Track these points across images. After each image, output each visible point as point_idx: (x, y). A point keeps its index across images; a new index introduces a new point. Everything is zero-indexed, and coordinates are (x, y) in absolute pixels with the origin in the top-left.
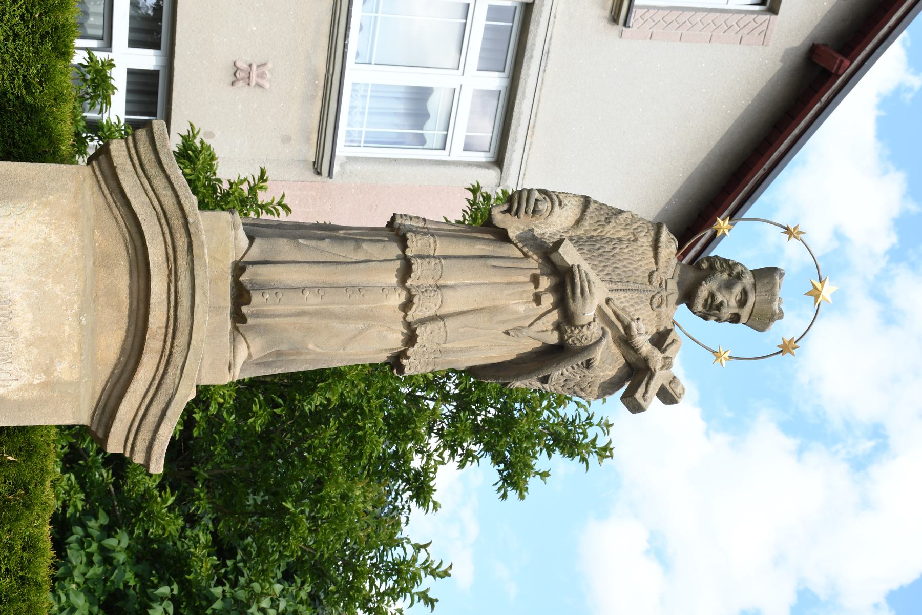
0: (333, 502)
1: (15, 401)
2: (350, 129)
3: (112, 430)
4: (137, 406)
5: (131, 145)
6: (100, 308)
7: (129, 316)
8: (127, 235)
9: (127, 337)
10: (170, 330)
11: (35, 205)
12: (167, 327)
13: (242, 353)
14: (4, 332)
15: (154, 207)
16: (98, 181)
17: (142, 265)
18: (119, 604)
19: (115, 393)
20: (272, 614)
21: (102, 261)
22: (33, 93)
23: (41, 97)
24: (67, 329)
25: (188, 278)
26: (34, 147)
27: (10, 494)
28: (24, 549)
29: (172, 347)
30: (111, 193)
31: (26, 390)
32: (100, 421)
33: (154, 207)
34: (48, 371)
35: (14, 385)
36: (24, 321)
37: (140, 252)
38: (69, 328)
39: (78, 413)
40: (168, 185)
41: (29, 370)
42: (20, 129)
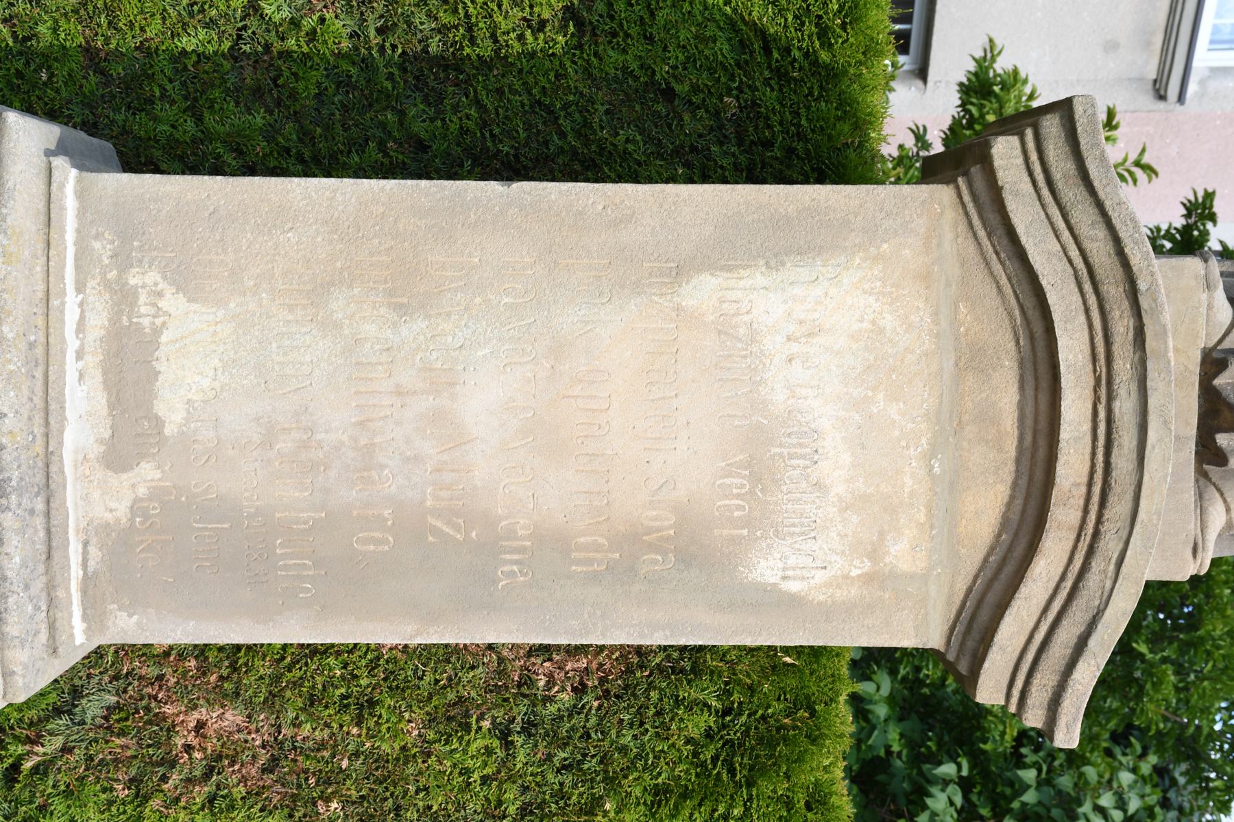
0: (1219, 648)
1: (820, 603)
2: (1218, 21)
3: (986, 665)
4: (1031, 625)
5: (1031, 145)
6: (965, 444)
7: (1018, 461)
8: (1017, 312)
9: (1012, 497)
10: (1097, 489)
11: (858, 261)
12: (1090, 484)
13: (1217, 518)
14: (804, 485)
15: (1070, 261)
16: (967, 214)
17: (1043, 368)
18: (881, 778)
19: (992, 598)
20: (1117, 815)
21: (971, 360)
22: (831, 45)
23: (842, 53)
24: (908, 481)
25: (1135, 394)
26: (830, 137)
27: (787, 716)
28: (808, 807)
29: (1099, 521)
30: (989, 235)
31: (839, 586)
32: (962, 644)
33: (1070, 261)
34: (875, 554)
35: (820, 577)
36: (837, 467)
37: (1041, 344)
38: (911, 480)
39: (919, 626)
40: (1099, 219)
41: (843, 552)
42: (808, 108)
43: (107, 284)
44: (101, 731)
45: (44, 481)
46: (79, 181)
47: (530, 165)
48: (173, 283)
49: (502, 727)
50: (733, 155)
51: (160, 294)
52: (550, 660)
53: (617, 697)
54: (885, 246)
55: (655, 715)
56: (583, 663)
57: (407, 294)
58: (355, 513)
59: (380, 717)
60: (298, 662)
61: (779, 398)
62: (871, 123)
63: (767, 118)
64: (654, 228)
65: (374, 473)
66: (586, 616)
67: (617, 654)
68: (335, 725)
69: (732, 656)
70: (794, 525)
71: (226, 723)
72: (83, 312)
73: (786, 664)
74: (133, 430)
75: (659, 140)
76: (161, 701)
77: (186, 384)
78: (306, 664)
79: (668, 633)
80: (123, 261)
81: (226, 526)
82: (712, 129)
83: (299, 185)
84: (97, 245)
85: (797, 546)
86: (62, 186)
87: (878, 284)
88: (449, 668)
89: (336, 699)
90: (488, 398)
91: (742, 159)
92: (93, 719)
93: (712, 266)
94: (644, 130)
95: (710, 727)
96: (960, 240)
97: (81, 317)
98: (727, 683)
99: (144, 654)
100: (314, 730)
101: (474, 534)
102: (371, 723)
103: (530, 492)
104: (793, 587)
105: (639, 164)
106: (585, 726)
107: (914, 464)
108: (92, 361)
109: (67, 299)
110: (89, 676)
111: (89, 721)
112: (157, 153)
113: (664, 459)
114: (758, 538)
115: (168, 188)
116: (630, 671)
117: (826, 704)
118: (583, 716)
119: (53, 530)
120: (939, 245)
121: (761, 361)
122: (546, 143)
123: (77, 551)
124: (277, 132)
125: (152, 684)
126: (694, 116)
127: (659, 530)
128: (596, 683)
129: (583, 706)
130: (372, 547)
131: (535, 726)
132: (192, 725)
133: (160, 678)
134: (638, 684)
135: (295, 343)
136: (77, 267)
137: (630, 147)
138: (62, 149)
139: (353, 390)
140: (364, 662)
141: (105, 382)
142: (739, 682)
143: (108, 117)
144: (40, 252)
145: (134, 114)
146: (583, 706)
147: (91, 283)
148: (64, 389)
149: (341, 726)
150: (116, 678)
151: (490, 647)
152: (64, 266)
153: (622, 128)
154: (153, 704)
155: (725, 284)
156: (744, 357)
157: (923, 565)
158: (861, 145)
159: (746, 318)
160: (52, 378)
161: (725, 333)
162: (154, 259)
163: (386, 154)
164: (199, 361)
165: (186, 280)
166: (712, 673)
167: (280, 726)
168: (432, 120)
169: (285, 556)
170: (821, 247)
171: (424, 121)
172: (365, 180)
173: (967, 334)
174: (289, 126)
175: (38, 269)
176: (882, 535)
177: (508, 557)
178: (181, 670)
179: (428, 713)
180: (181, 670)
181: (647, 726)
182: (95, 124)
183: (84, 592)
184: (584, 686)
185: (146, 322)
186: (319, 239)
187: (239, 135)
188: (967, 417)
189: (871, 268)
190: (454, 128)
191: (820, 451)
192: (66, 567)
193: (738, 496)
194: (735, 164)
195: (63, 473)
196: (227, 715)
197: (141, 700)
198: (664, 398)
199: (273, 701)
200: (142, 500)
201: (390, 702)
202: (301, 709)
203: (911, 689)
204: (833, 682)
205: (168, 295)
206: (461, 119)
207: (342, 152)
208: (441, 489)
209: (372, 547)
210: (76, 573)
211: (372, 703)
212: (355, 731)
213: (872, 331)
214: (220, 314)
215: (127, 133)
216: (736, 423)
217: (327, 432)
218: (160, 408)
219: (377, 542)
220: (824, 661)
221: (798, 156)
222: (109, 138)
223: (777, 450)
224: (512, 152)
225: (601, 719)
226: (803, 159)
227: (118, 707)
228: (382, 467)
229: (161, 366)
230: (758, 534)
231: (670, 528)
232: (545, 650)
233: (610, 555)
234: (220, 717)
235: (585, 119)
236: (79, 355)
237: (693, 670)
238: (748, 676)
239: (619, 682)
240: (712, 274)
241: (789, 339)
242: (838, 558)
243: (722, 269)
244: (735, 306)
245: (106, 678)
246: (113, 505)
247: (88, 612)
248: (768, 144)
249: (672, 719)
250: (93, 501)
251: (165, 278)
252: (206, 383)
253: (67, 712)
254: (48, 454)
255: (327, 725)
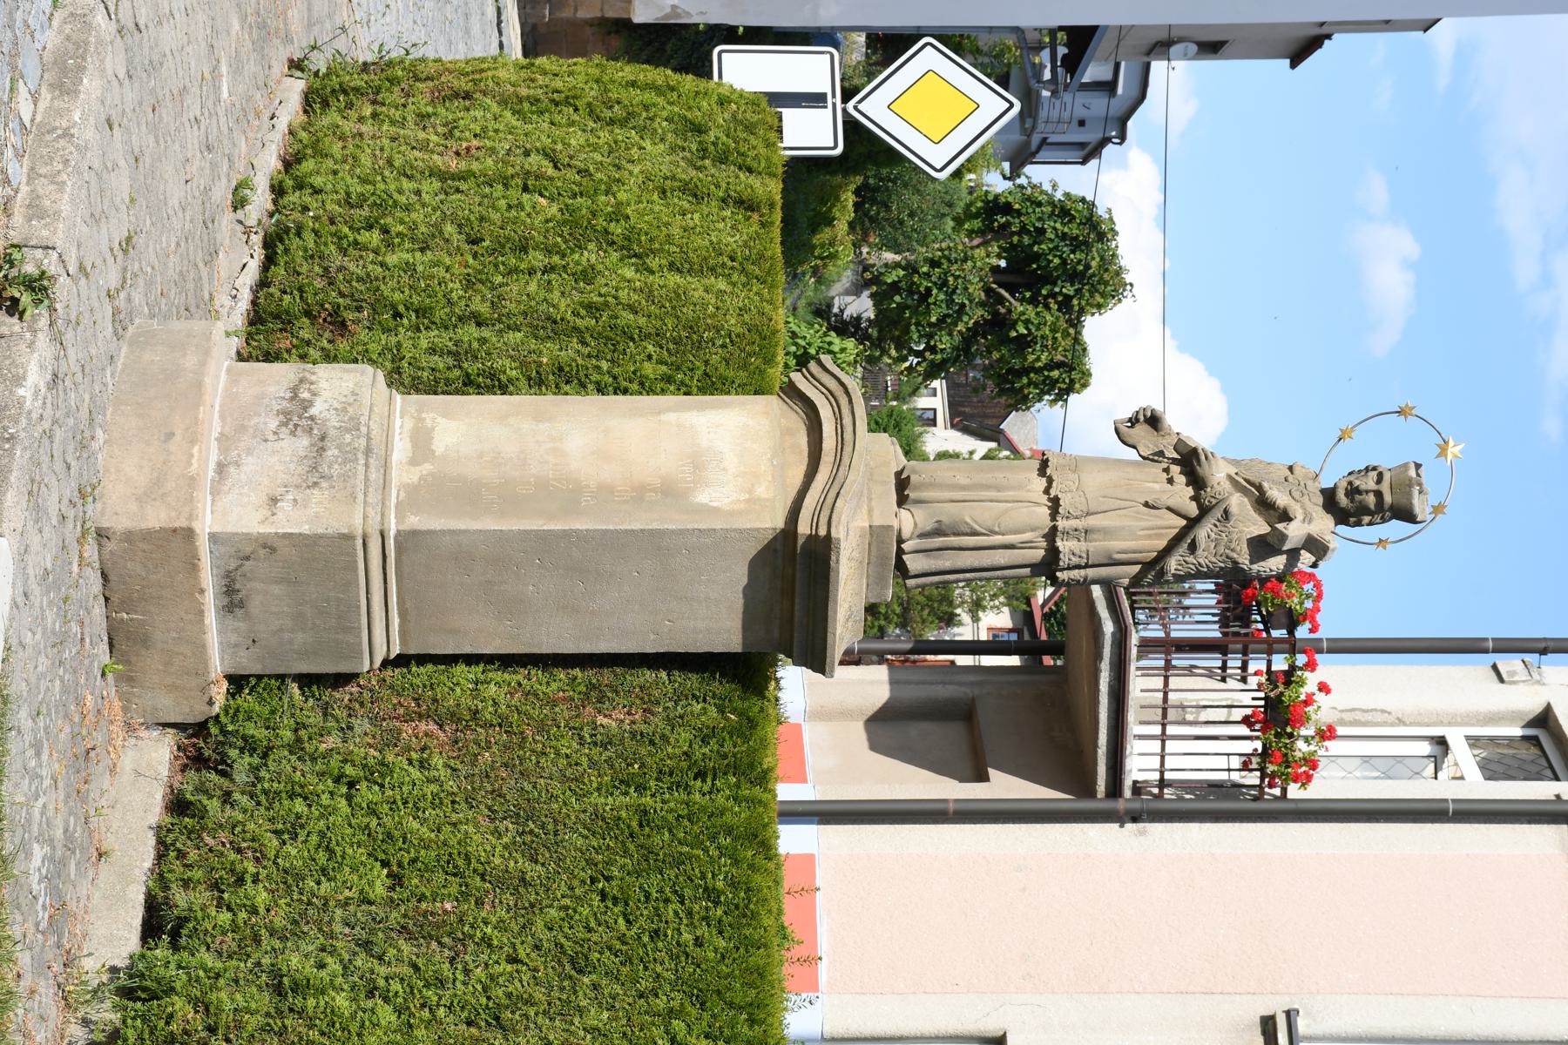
104: (715, 504)
210: (394, 500)
250: (402, 473)
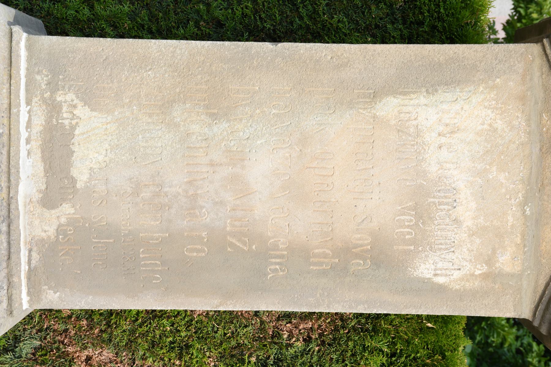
11: (481, 89)
14: (447, 220)
24: (510, 219)
26: (458, 19)
27: (429, 358)
31: (468, 280)
34: (490, 261)
35: (457, 275)
36: (467, 210)
38: (512, 218)
41: (471, 260)
43: (44, 100)
44: (31, 362)
45: (7, 214)
46: (28, 40)
47: (282, 35)
48: (82, 100)
49: (262, 362)
50: (400, 30)
51: (75, 107)
52: (290, 322)
53: (329, 345)
54: (498, 80)
55: (351, 356)
56: (310, 325)
57: (217, 107)
58: (186, 234)
59: (192, 354)
60: (145, 322)
61: (433, 169)
62: (482, 11)
63: (421, 8)
64: (360, 70)
65: (197, 211)
66: (318, 295)
67: (329, 320)
68: (166, 359)
69: (396, 322)
70: (441, 244)
71: (104, 357)
72: (30, 116)
73: (428, 328)
74: (58, 185)
75: (357, 21)
76: (66, 344)
77: (88, 159)
78: (150, 323)
79: (366, 306)
80: (53, 86)
81: (111, 241)
82: (388, 15)
83: (155, 44)
84: (38, 77)
85: (443, 256)
86: (18, 43)
87: (494, 102)
88: (232, 326)
89: (167, 344)
90: (263, 168)
91: (405, 32)
92: (26, 355)
93: (394, 92)
94: (349, 15)
95: (383, 364)
96: (544, 76)
97: (29, 119)
98: (393, 338)
99: (56, 317)
100: (154, 361)
101: (254, 247)
102: (187, 358)
103: (287, 223)
104: (441, 280)
105: (346, 35)
106: (310, 362)
107: (514, 209)
108: (35, 145)
109: (21, 109)
110: (25, 330)
111: (24, 356)
112: (68, 27)
113: (367, 204)
114: (420, 251)
115: (80, 44)
116: (336, 330)
117: (451, 351)
118: (309, 356)
119: (12, 242)
120: (531, 79)
121: (423, 148)
122: (292, 23)
123: (25, 255)
124: (137, 15)
125: (61, 334)
126: (378, 7)
127: (361, 246)
128: (317, 336)
129: (310, 350)
130: (195, 254)
131: (281, 361)
132: (84, 358)
133: (66, 331)
134: (341, 338)
135: (152, 136)
136: (27, 91)
137: (340, 25)
138: (16, 22)
139: (185, 163)
140: (183, 323)
141: (43, 157)
142: (400, 338)
143: (39, 5)
144: (5, 81)
145: (54, 4)
146: (310, 350)
147: (35, 100)
148: (19, 161)
149: (170, 360)
150: (40, 331)
151: (256, 313)
152: (20, 89)
153: (336, 14)
154: (61, 346)
155: (402, 102)
156: (413, 145)
157: (519, 268)
158: (476, 24)
159: (414, 123)
160: (12, 154)
161: (402, 131)
162: (71, 86)
163: (199, 29)
164: (98, 144)
165: (89, 99)
166: (385, 332)
167: (134, 359)
168: (226, 9)
169: (144, 259)
170: (459, 81)
171: (221, 10)
172: (193, 41)
173: (547, 132)
174: (144, 12)
175: (5, 91)
176: (494, 251)
177: (274, 260)
178: (78, 326)
179: (220, 353)
180: (78, 326)
181: (347, 362)
182: (31, 10)
183: (29, 278)
184: (310, 338)
185: (66, 122)
186: (167, 76)
187: (115, 17)
188: (547, 181)
189: (489, 93)
190: (238, 13)
191: (458, 201)
192: (19, 264)
193: (408, 227)
194: (401, 35)
195: (18, 209)
196: (104, 353)
197: (54, 344)
198: (366, 169)
199: (130, 345)
200: (63, 225)
201: (198, 346)
202: (147, 349)
203: (482, 348)
204: (455, 339)
205: (79, 107)
206: (242, 9)
207: (174, 27)
208: (235, 221)
209: (195, 254)
210: (24, 267)
211: (188, 347)
212: (178, 362)
213: (489, 130)
214: (109, 118)
215: (50, 15)
216: (408, 184)
217: (170, 187)
218: (74, 172)
219: (198, 251)
220: (450, 326)
221: (438, 30)
222: (40, 18)
223: (432, 200)
224: (272, 28)
225: (320, 358)
226: (441, 32)
227: (41, 348)
228: (202, 207)
229: (75, 148)
230: (420, 249)
231: (368, 245)
232: (288, 316)
233: (333, 260)
234: (100, 354)
235: (314, 9)
236: (28, 141)
237: (374, 330)
238: (406, 334)
239: (330, 336)
240: (394, 97)
241: (439, 135)
242: (467, 264)
243: (400, 94)
244: (408, 115)
245: (34, 331)
246: (46, 228)
247: (31, 290)
248: (421, 23)
249: (361, 359)
251: (77, 97)
252: (101, 158)
253: (11, 350)
254: (9, 198)
255: (162, 359)
